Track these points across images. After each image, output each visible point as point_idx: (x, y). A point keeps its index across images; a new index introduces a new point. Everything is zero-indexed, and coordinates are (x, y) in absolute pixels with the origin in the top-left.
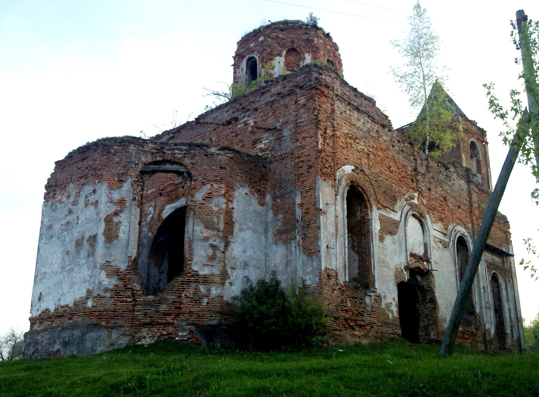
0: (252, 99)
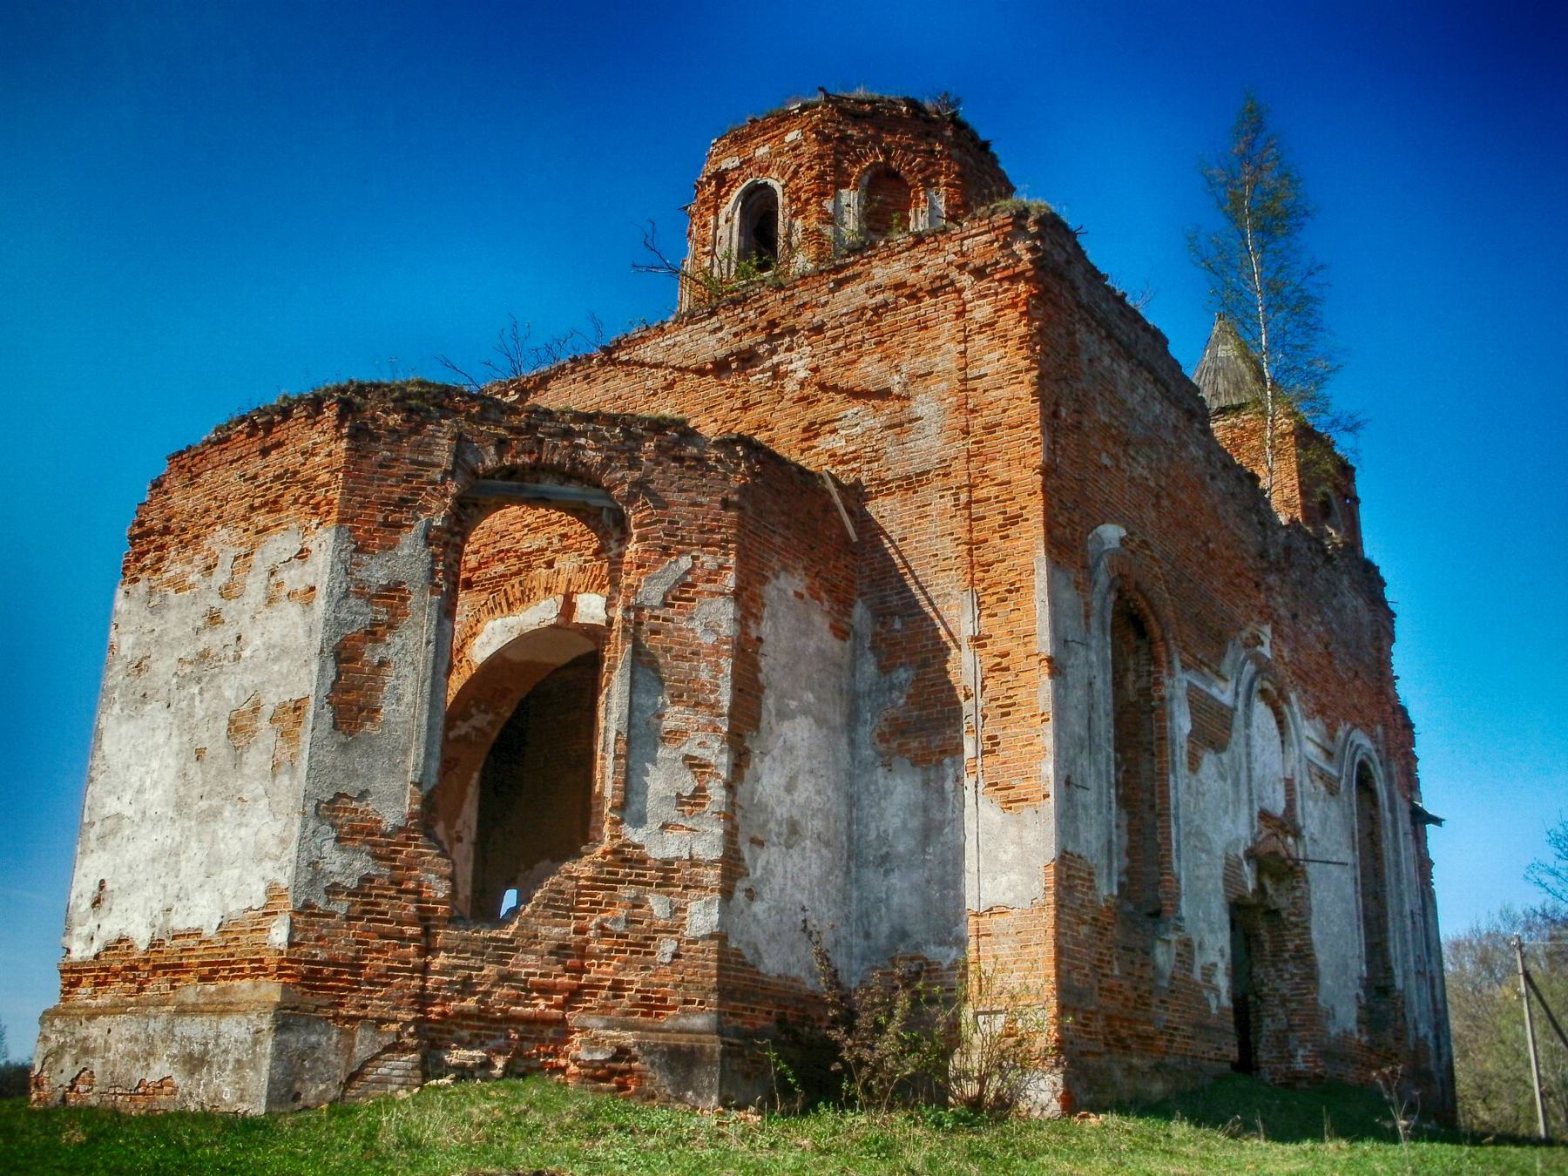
0: (806, 298)
